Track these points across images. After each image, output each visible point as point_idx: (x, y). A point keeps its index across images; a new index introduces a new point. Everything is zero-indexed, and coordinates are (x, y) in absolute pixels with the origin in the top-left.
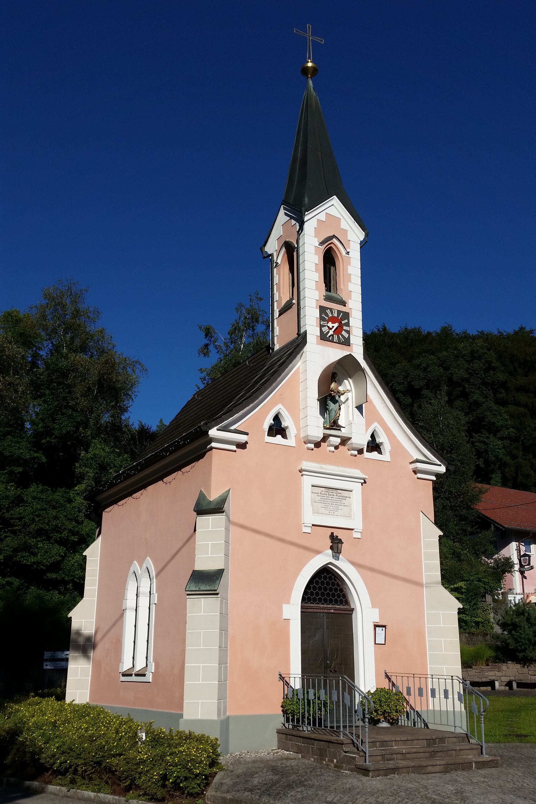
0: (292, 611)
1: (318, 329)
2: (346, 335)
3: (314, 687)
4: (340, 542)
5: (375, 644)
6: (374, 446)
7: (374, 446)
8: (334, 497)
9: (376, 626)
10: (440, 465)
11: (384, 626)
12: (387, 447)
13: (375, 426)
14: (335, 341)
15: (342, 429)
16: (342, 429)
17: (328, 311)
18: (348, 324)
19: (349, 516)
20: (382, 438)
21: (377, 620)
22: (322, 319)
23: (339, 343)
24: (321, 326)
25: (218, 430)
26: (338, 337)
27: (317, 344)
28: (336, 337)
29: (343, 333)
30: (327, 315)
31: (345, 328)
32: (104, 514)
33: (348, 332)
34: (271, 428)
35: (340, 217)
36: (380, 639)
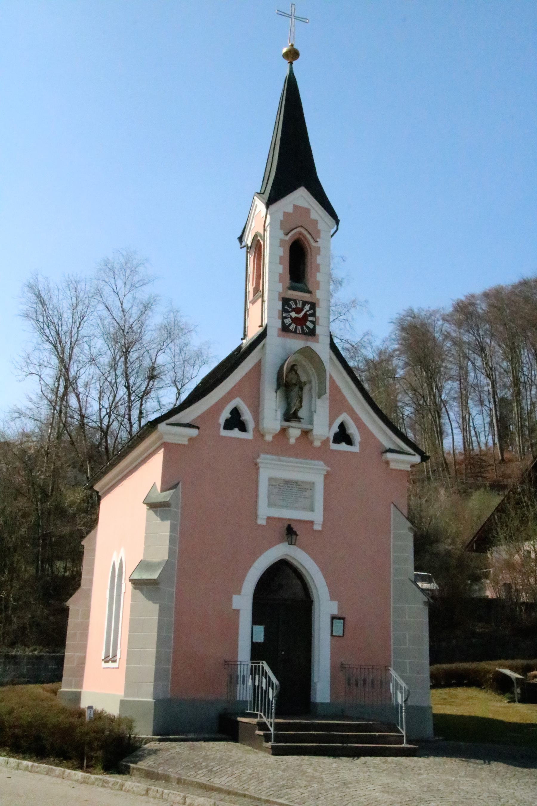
0: (243, 602)
1: (280, 322)
2: (311, 326)
3: (259, 674)
4: (295, 533)
5: (332, 635)
6: (343, 436)
7: (343, 436)
8: (294, 488)
9: (333, 618)
10: (414, 455)
11: (343, 619)
12: (356, 436)
13: (344, 417)
14: (298, 332)
15: (302, 420)
16: (302, 420)
17: (292, 303)
18: (314, 315)
19: (312, 510)
20: (353, 430)
21: (335, 612)
22: (284, 310)
23: (303, 333)
24: (283, 318)
25: (167, 424)
26: (302, 329)
27: (279, 336)
28: (299, 328)
29: (308, 324)
30: (290, 306)
31: (310, 318)
32: (166, 558)
33: (313, 323)
34: (227, 421)
35: (309, 207)
36: (338, 631)
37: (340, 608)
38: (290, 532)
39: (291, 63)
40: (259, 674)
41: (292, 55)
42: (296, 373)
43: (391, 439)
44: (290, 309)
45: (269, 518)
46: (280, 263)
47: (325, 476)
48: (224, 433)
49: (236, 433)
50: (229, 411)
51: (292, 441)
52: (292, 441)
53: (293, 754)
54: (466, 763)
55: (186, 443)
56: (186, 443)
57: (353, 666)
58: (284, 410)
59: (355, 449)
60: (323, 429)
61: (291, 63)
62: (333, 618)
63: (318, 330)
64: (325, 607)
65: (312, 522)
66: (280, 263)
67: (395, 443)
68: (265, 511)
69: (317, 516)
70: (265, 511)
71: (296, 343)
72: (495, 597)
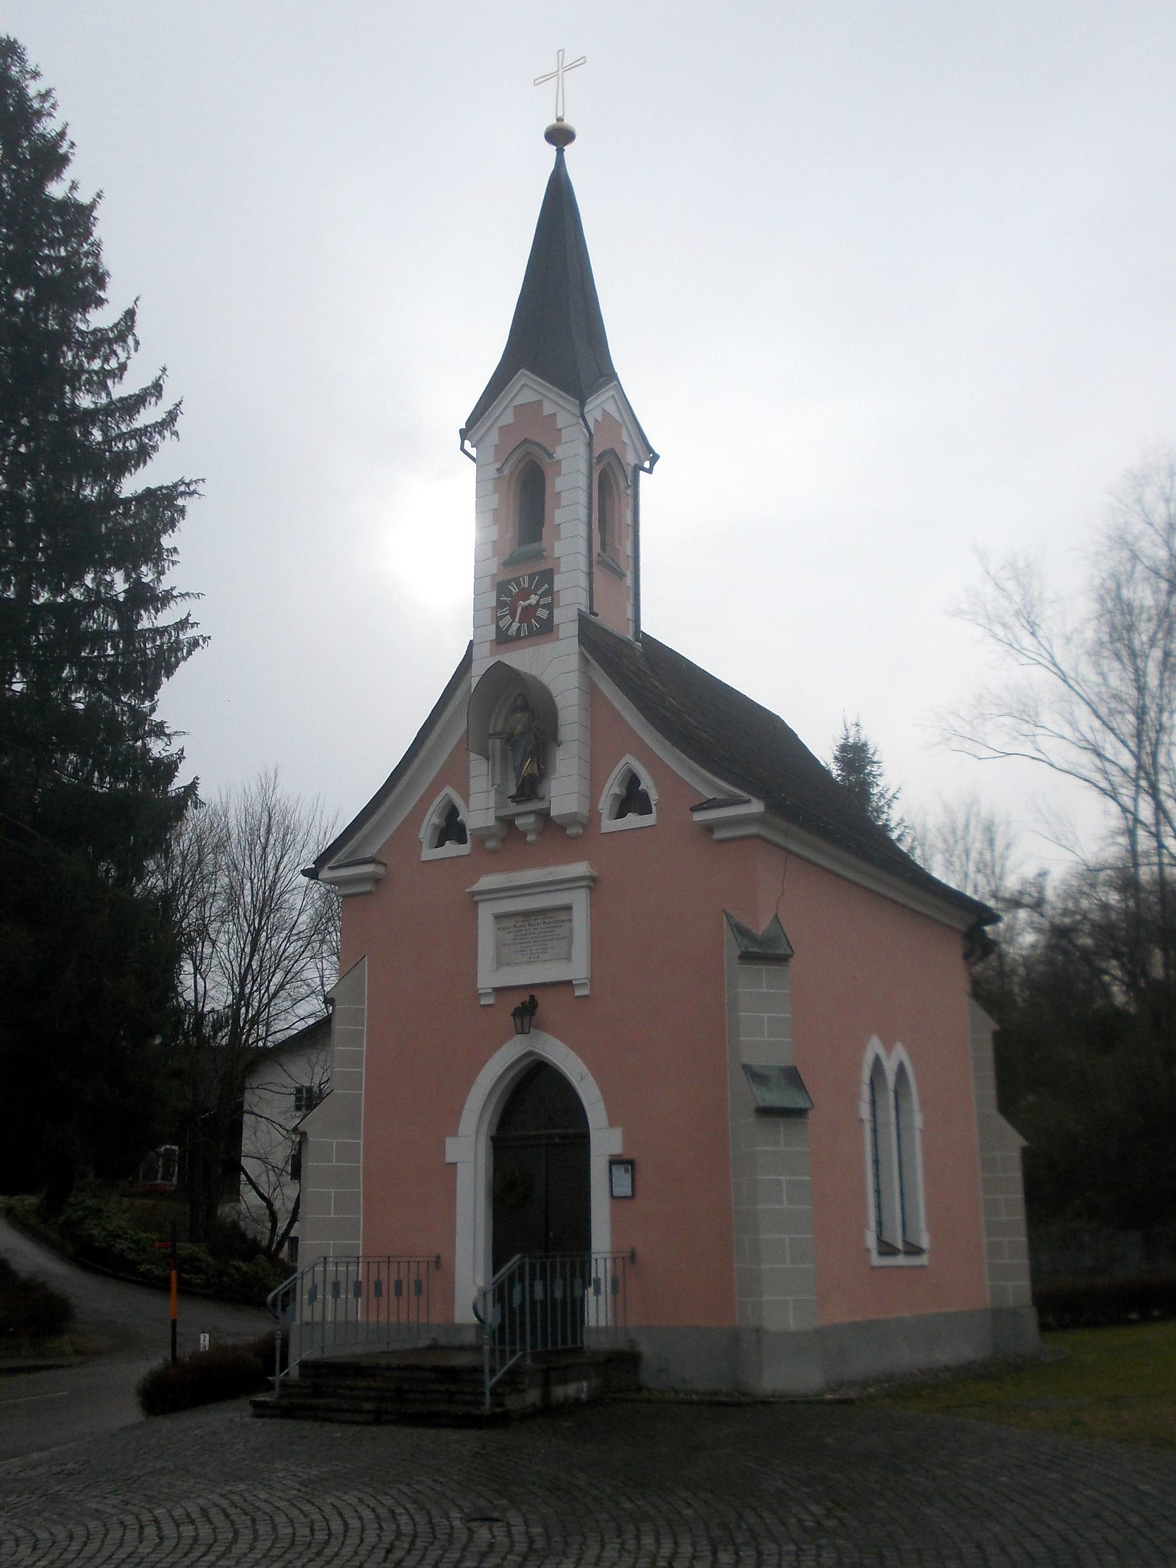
3: (533, 1302)
5: (612, 1196)
7: (632, 799)
13: (630, 761)
37: (628, 1141)
39: (560, 152)
40: (533, 1302)
41: (560, 136)
43: (713, 786)
45: (497, 990)
46: (495, 492)
57: (419, 1259)
61: (560, 152)
64: (605, 1141)
65: (569, 983)
66: (495, 492)
67: (721, 790)
68: (489, 977)
69: (577, 968)
70: (489, 977)
72: (259, 966)
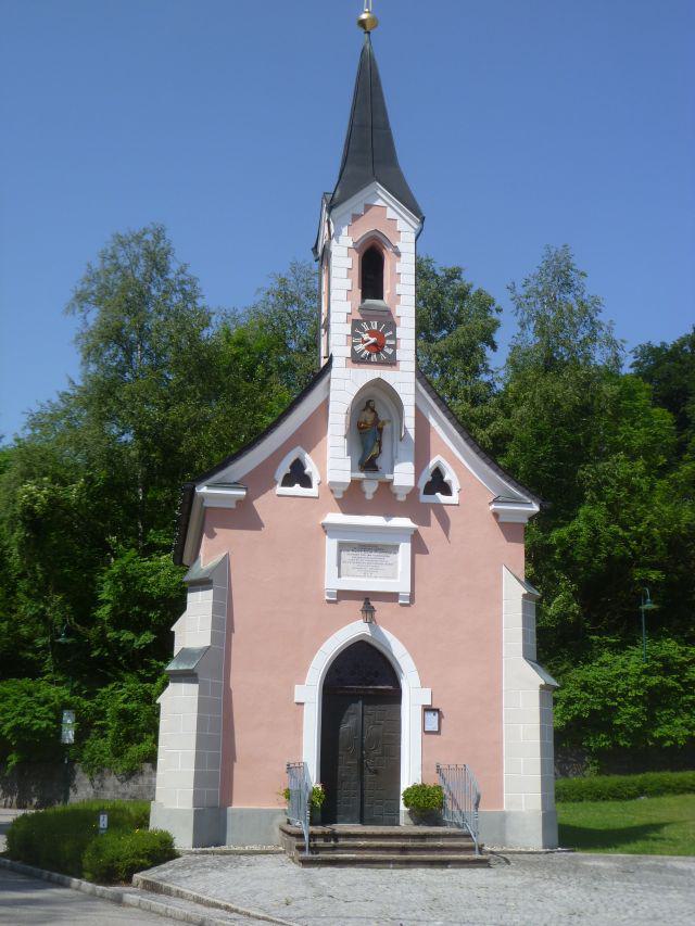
0: (309, 693)
2: (390, 351)
22: (354, 335)
30: (362, 330)
31: (388, 342)
34: (287, 476)
38: (369, 602)
42: (373, 411)
44: (367, 329)
47: (412, 536)
48: (455, 487)
49: (297, 489)
50: (290, 463)
51: (369, 496)
52: (369, 496)
53: (216, 623)
54: (36, 409)
55: (233, 506)
56: (233, 506)
58: (360, 456)
59: (313, 491)
60: (403, 475)
62: (427, 709)
63: (399, 356)
71: (368, 374)
